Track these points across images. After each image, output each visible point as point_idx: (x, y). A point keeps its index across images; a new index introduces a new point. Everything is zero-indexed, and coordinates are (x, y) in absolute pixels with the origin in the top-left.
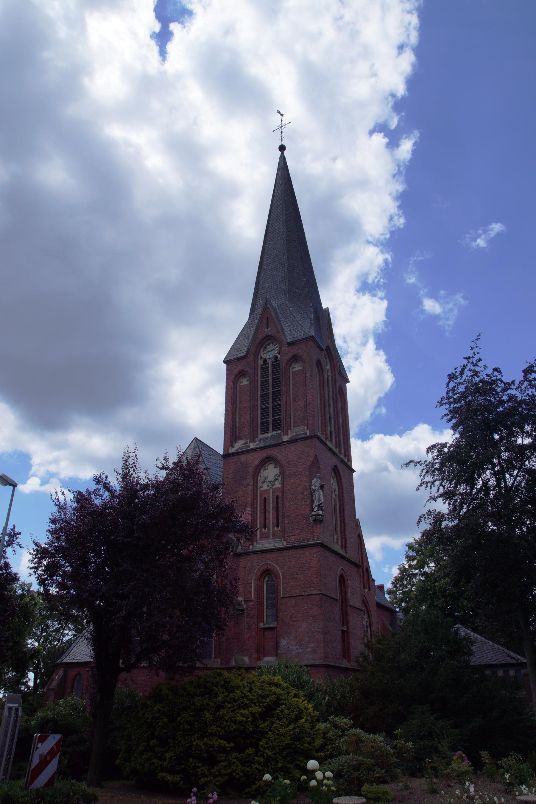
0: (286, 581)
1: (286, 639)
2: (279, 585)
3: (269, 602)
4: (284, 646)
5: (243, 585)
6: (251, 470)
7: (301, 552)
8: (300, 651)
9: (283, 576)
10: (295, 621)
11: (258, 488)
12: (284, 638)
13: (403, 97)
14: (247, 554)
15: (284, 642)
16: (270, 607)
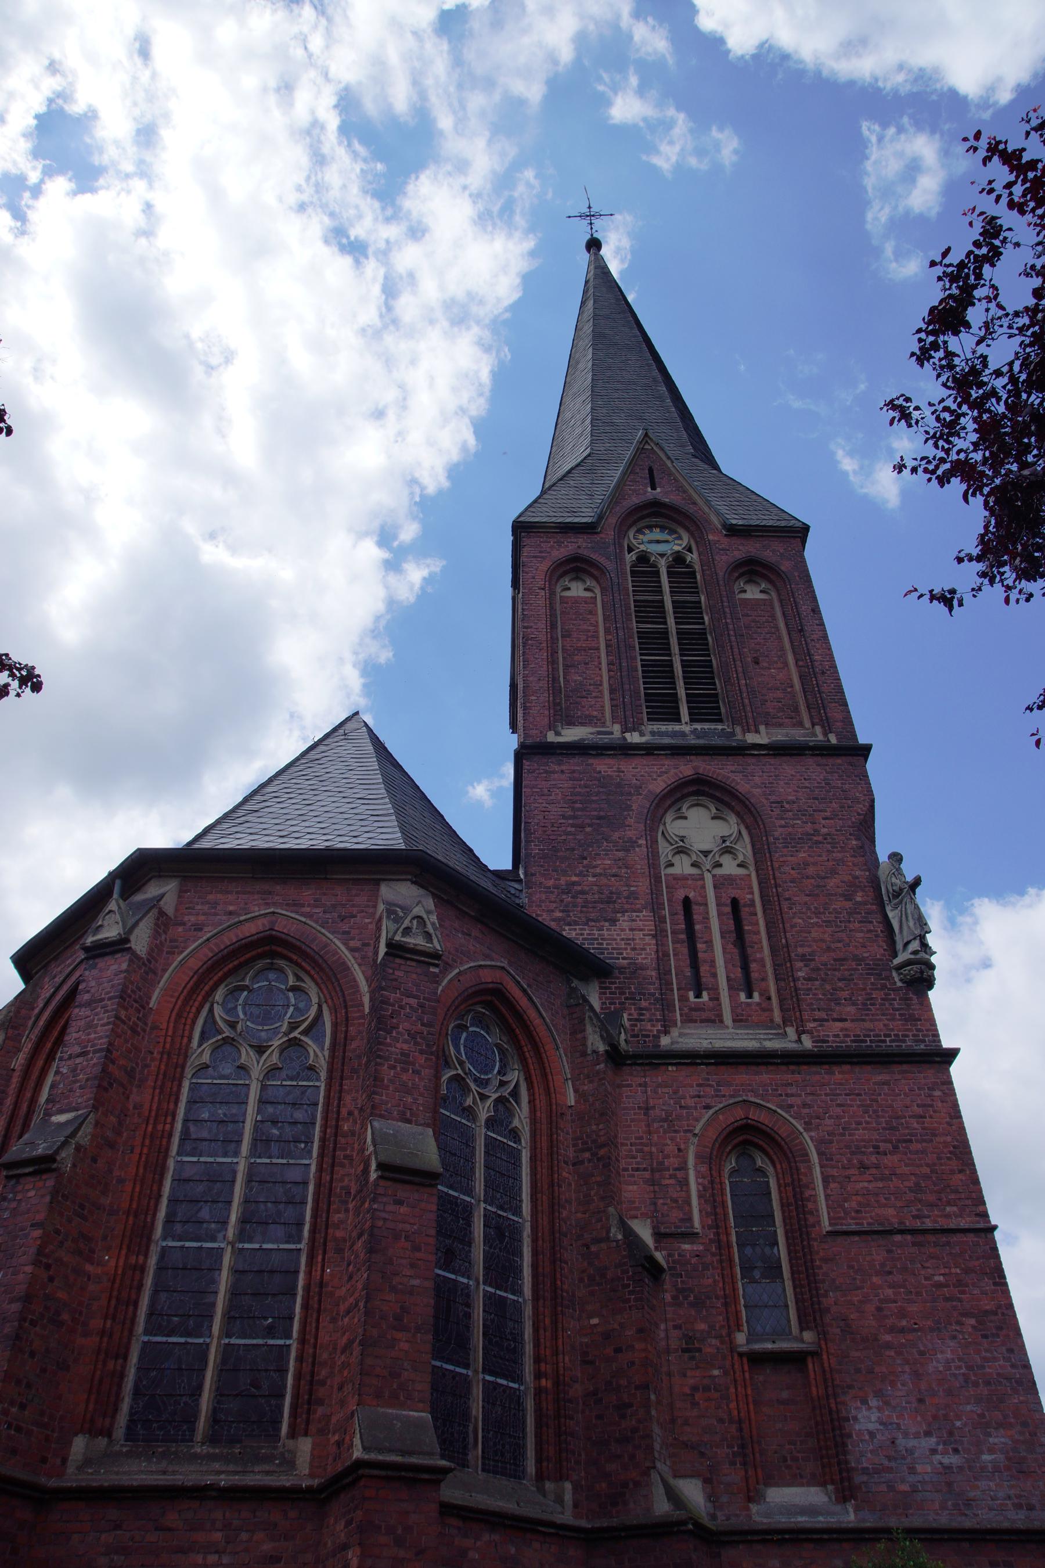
0: (834, 1172)
1: (873, 1402)
2: (810, 1185)
3: (748, 1251)
4: (872, 1434)
5: (647, 1175)
6: (639, 804)
7: (880, 1078)
8: (953, 1460)
9: (820, 1154)
10: (902, 1330)
11: (189, 1072)
12: (864, 1401)
13: (440, 493)
14: (657, 1059)
15: (866, 1419)
16: (757, 1274)
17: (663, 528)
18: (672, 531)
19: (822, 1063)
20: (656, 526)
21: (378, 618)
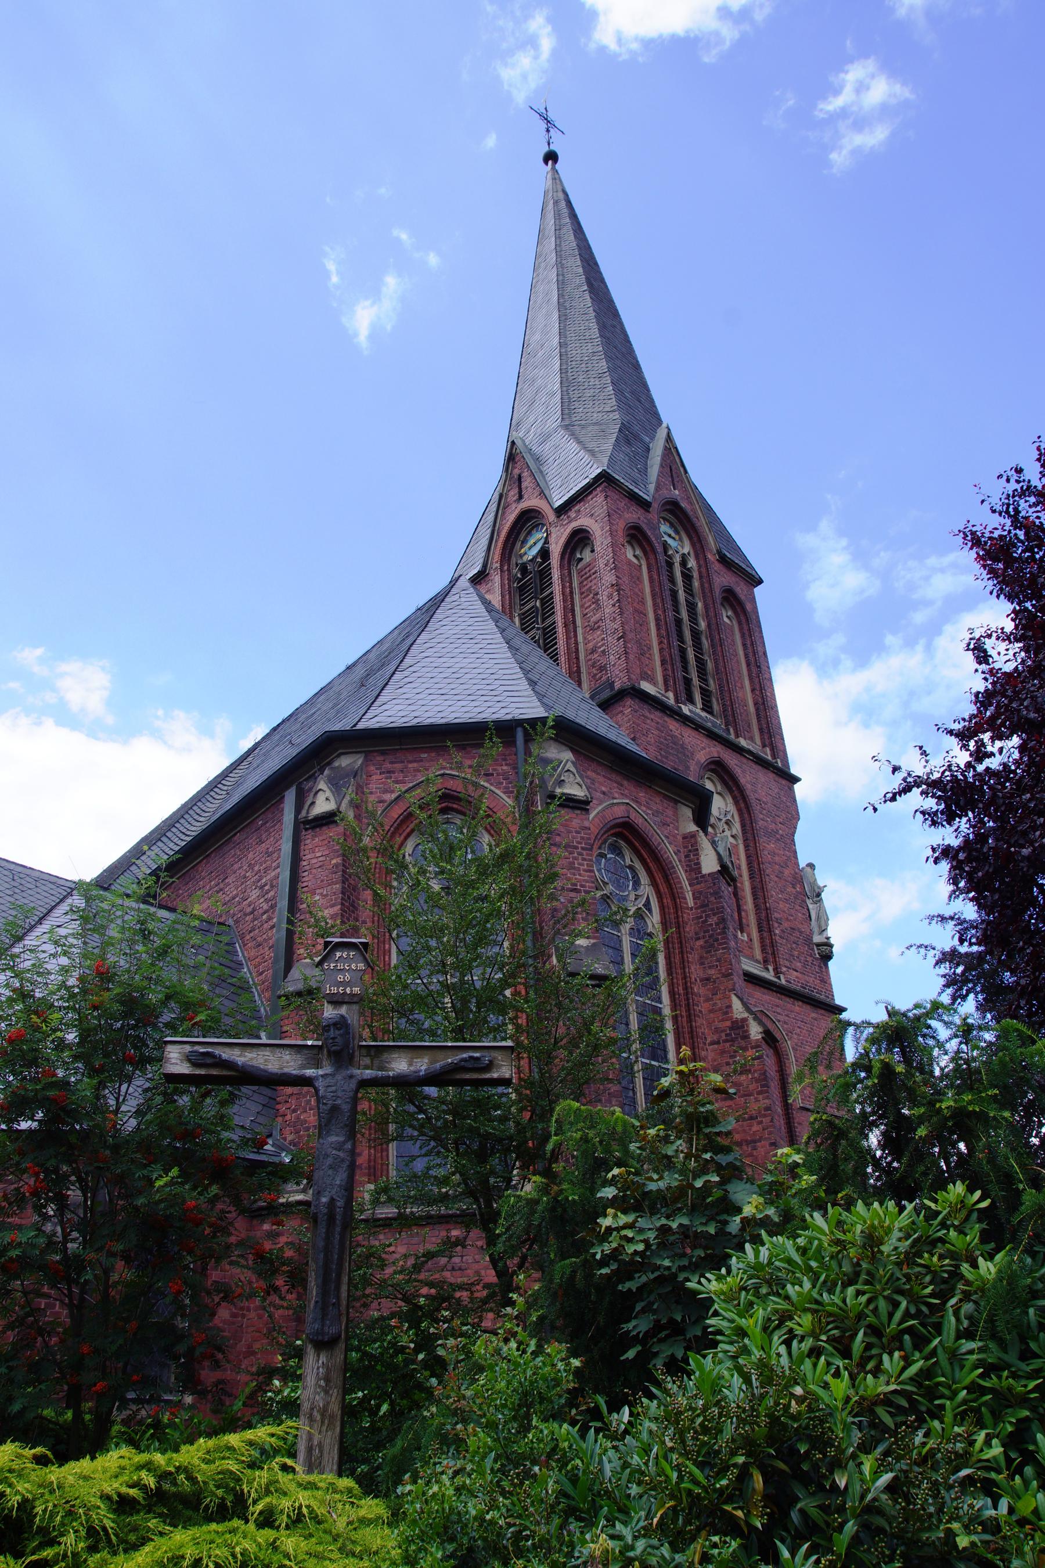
17: (672, 525)
18: (677, 532)
19: (790, 997)
20: (668, 521)
21: (661, 36)
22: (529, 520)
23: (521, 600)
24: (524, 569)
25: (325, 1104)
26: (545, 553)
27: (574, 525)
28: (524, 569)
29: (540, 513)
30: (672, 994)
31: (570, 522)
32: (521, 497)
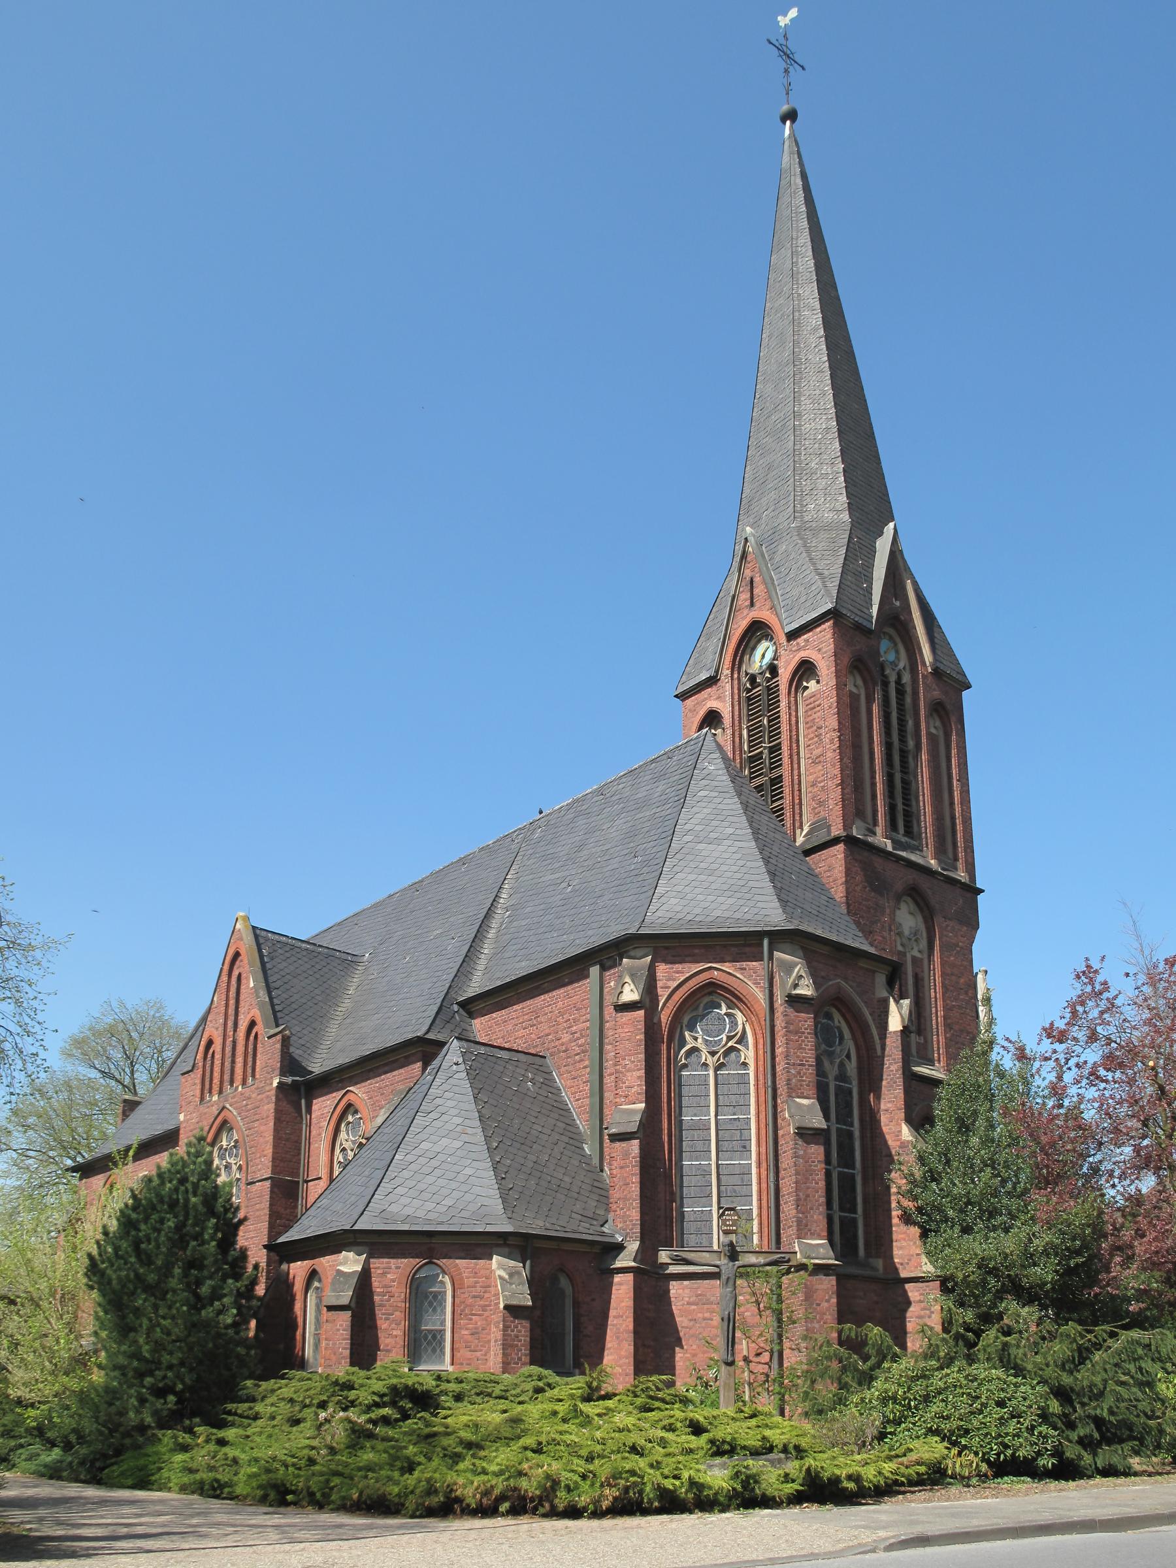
22: (759, 629)
23: (749, 705)
24: (752, 679)
25: (1168, 1388)
26: (773, 669)
27: (803, 654)
28: (752, 679)
29: (770, 628)
30: (862, 1121)
31: (798, 650)
32: (752, 604)
